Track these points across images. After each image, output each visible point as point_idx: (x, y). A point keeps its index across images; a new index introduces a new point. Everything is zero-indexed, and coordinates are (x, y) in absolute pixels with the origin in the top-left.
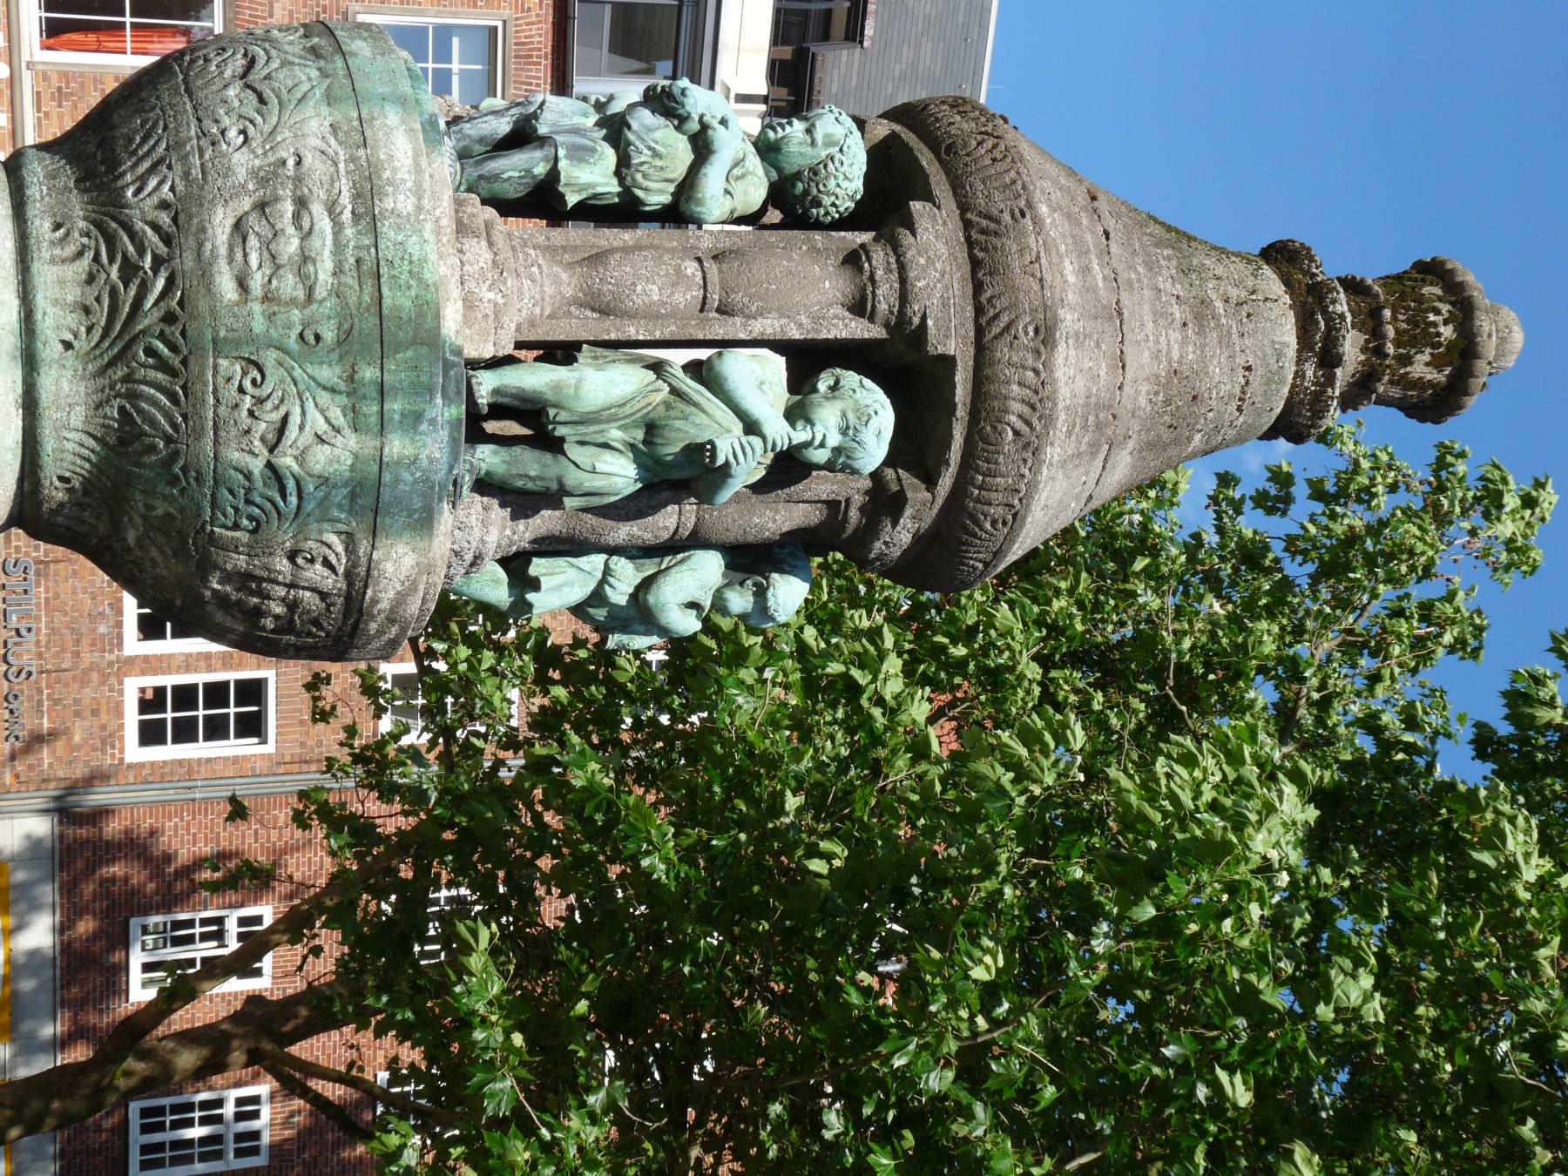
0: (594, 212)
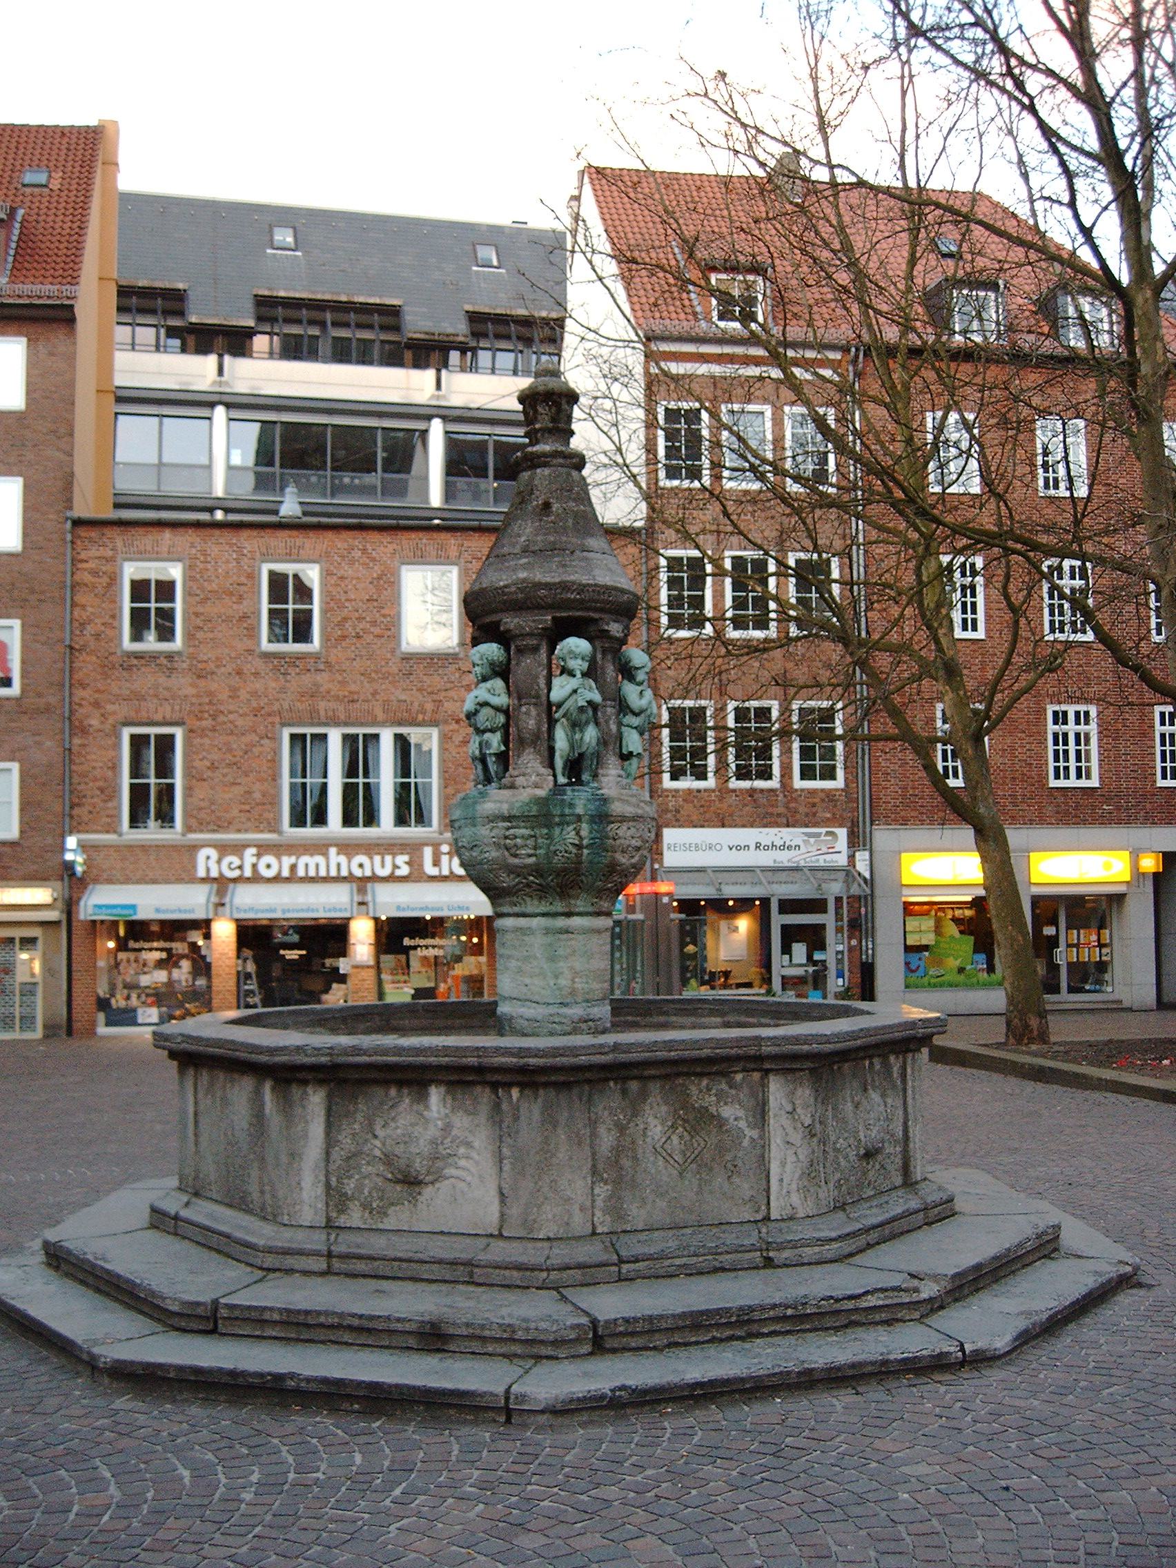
0: (506, 741)
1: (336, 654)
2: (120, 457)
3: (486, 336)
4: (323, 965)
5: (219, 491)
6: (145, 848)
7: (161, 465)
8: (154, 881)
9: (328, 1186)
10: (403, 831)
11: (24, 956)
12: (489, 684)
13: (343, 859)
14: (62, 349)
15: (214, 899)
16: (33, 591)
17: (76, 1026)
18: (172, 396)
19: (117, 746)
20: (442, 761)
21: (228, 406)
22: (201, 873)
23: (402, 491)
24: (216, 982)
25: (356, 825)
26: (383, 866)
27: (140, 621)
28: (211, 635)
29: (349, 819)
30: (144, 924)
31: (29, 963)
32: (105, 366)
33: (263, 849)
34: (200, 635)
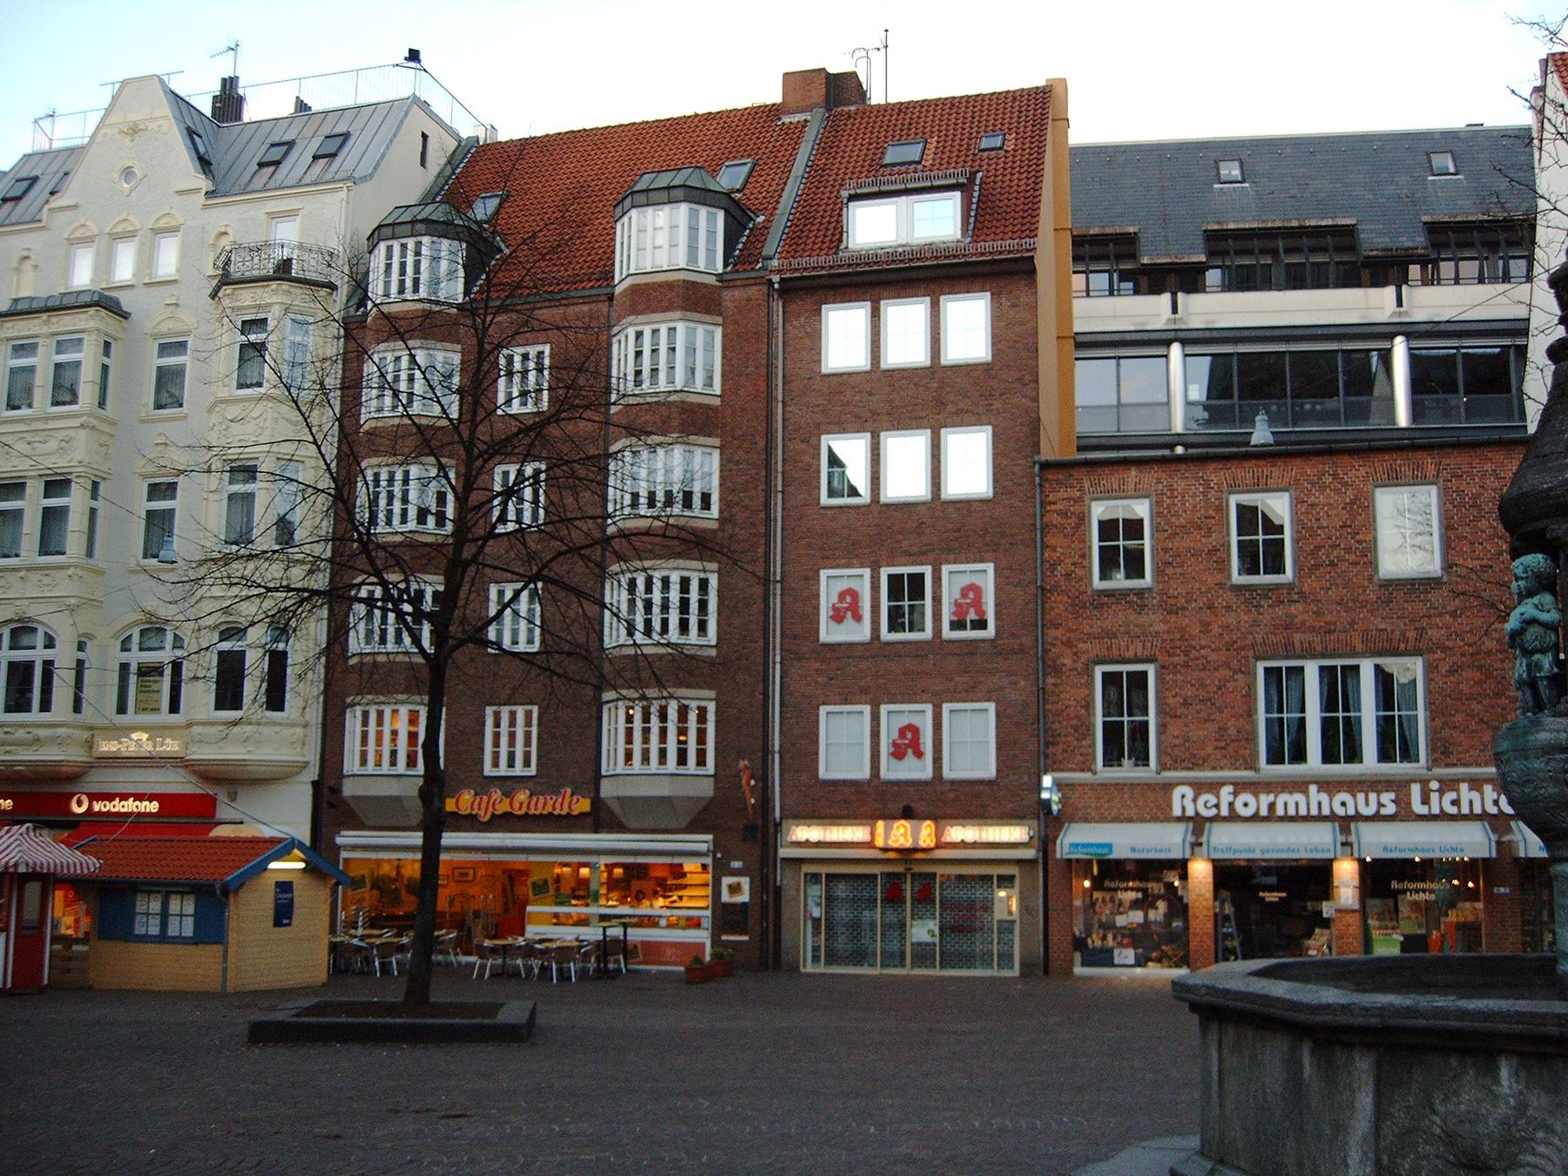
1: (1310, 584)
2: (1077, 403)
3: (1446, 246)
4: (1305, 908)
5: (1178, 426)
6: (1118, 786)
7: (1119, 405)
8: (1130, 820)
9: (1378, 1163)
10: (1388, 768)
11: (1002, 894)
12: (1535, 600)
13: (1324, 797)
14: (1023, 299)
15: (1190, 839)
16: (1003, 535)
17: (1053, 965)
18: (1128, 337)
19: (1090, 685)
20: (1428, 692)
21: (1184, 342)
22: (1177, 812)
23: (1363, 413)
24: (1192, 923)
25: (1282, 762)
26: (1367, 804)
27: (1109, 561)
28: (1179, 570)
29: (1329, 756)
30: (1120, 863)
31: (1007, 901)
32: (1065, 314)
33: (1240, 787)
34: (1169, 571)
